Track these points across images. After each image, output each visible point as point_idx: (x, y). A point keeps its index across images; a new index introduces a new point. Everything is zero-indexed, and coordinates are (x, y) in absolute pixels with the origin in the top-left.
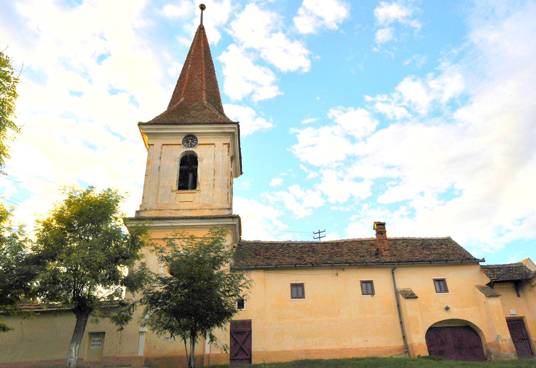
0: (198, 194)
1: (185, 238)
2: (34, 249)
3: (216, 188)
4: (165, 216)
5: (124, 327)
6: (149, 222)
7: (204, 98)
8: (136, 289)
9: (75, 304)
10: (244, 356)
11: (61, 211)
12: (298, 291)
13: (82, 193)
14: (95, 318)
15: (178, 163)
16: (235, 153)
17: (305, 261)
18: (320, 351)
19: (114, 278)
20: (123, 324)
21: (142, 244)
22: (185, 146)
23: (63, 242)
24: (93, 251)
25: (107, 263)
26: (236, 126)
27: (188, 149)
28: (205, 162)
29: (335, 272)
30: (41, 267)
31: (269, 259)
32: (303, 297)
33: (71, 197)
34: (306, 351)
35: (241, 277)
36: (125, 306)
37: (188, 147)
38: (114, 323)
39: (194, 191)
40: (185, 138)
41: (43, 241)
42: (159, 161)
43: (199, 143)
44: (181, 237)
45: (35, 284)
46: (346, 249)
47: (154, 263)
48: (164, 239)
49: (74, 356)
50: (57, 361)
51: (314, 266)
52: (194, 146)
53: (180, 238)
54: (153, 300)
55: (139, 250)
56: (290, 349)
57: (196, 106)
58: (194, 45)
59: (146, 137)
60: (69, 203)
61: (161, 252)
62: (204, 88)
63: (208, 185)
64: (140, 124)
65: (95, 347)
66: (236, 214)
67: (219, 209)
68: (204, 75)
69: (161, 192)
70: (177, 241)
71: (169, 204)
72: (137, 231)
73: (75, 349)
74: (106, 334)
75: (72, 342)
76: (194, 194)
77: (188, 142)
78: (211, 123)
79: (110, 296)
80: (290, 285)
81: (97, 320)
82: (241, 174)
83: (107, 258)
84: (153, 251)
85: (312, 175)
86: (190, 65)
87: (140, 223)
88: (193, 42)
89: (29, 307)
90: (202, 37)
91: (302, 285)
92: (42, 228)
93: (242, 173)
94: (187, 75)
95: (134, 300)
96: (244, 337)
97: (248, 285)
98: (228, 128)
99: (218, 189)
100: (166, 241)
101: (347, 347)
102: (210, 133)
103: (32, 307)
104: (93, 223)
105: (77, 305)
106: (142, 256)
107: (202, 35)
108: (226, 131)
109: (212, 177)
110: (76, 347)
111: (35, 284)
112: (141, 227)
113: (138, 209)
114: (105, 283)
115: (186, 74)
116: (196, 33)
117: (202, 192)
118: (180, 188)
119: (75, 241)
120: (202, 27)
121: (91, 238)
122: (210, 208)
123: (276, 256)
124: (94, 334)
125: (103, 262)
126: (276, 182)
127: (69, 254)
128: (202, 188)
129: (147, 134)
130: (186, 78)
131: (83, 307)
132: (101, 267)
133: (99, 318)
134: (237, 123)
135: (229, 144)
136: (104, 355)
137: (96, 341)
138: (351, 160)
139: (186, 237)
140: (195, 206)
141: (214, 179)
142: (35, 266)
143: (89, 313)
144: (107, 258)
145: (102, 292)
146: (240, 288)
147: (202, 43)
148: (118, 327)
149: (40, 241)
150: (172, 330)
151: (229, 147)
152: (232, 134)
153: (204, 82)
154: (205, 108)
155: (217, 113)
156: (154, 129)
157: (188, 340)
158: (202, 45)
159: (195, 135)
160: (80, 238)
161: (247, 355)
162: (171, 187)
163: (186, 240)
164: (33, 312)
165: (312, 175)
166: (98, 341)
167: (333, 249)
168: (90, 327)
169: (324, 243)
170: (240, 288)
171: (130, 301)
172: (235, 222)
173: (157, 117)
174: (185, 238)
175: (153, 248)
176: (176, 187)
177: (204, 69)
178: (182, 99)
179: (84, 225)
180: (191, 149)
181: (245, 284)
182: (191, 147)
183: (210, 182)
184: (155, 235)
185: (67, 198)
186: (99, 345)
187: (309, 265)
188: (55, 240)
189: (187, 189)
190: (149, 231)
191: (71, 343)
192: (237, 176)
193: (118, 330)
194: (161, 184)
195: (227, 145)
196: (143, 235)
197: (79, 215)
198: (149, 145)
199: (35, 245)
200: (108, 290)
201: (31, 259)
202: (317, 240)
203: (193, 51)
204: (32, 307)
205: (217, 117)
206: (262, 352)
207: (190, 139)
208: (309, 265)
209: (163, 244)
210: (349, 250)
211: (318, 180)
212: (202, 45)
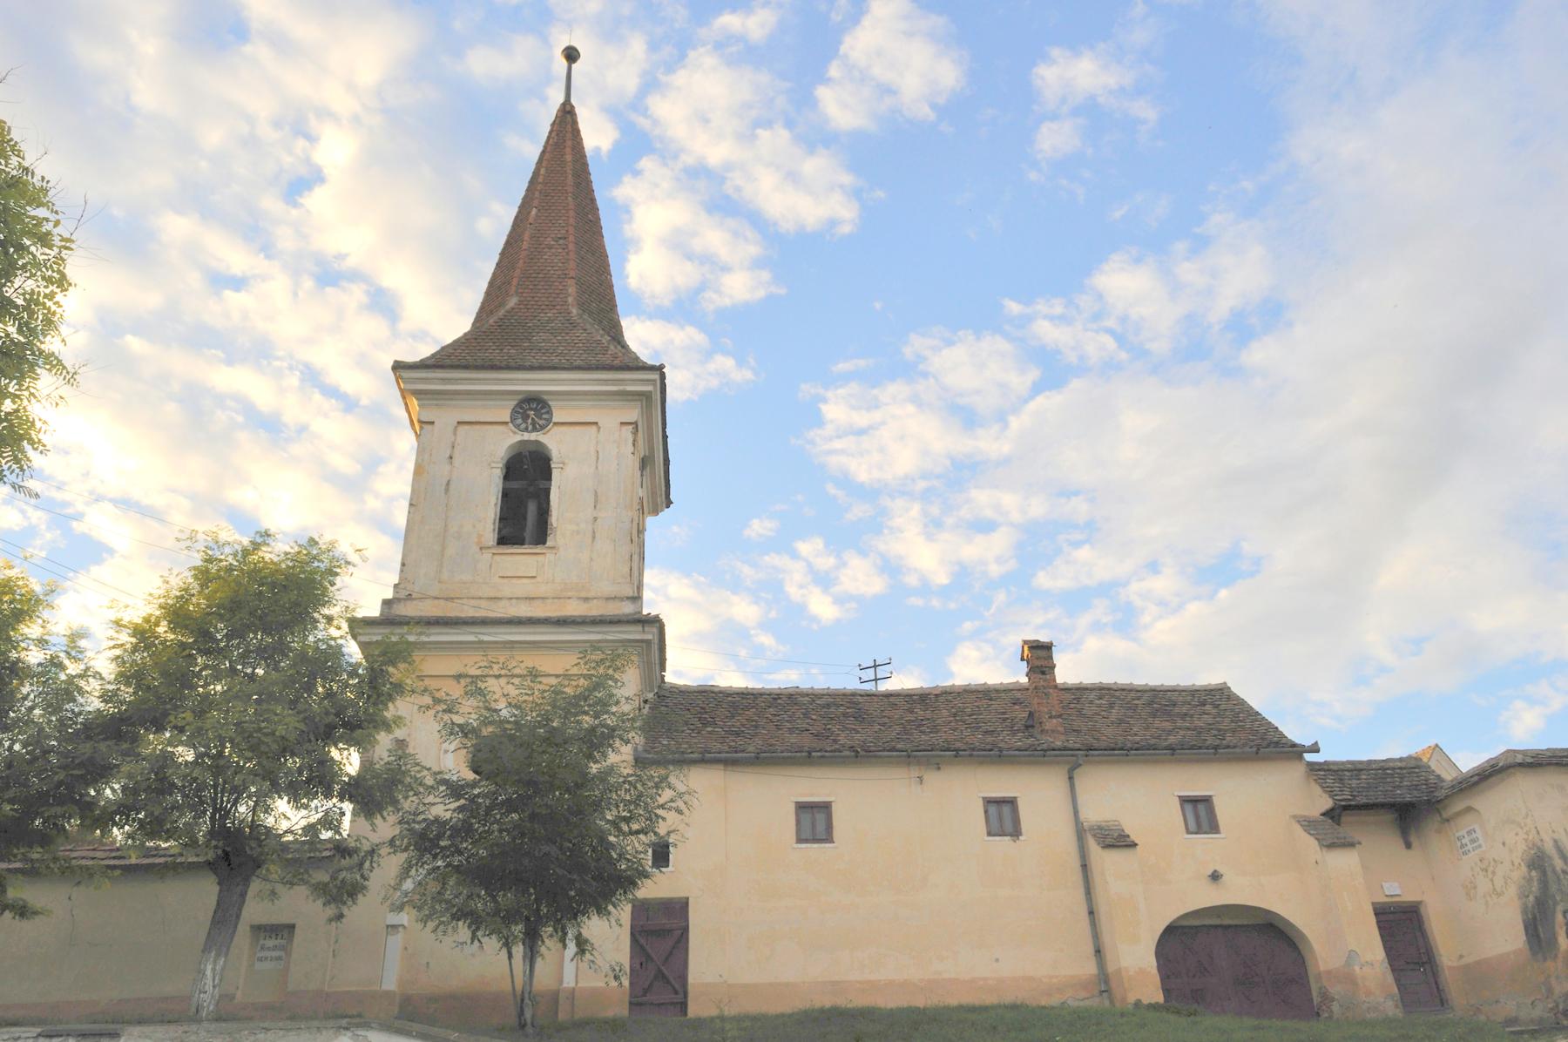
0: (550, 556)
1: (513, 676)
2: (106, 697)
5: (345, 911)
7: (570, 300)
9: (216, 847)
14: (269, 886)
15: (498, 473)
17: (835, 741)
19: (321, 780)
21: (399, 688)
22: (517, 427)
23: (185, 680)
24: (265, 706)
26: (656, 376)
27: (526, 436)
29: (915, 772)
30: (125, 746)
31: (738, 734)
32: (828, 838)
34: (834, 983)
38: (320, 902)
39: (539, 549)
42: (447, 467)
43: (555, 420)
45: (108, 792)
48: (458, 677)
51: (861, 756)
52: (542, 428)
54: (424, 840)
57: (550, 321)
58: (547, 156)
61: (449, 711)
62: (572, 274)
64: (398, 367)
67: (607, 599)
68: (571, 238)
70: (491, 681)
72: (384, 654)
73: (214, 970)
75: (206, 949)
76: (540, 558)
77: (525, 418)
79: (311, 829)
81: (273, 893)
83: (302, 726)
84: (428, 708)
86: (534, 211)
90: (569, 135)
92: (126, 638)
93: (669, 503)
94: (526, 237)
95: (375, 838)
97: (680, 804)
98: (634, 383)
101: (946, 976)
102: (586, 393)
103: (98, 854)
104: (266, 632)
105: (220, 852)
106: (398, 721)
107: (569, 128)
110: (215, 962)
111: (108, 792)
112: (396, 643)
114: (298, 792)
118: (502, 541)
119: (217, 678)
121: (260, 672)
122: (583, 595)
124: (261, 930)
125: (292, 737)
127: (200, 713)
129: (418, 394)
130: (525, 245)
131: (237, 857)
132: (286, 749)
133: (279, 888)
134: (661, 367)
135: (636, 424)
138: (963, 472)
140: (542, 590)
141: (595, 519)
144: (302, 726)
145: (288, 817)
147: (568, 150)
148: (331, 911)
149: (124, 678)
152: (646, 396)
154: (574, 325)
156: (435, 381)
157: (519, 950)
158: (569, 158)
160: (233, 670)
161: (676, 993)
162: (480, 536)
163: (516, 681)
165: (859, 511)
166: (275, 948)
168: (256, 909)
169: (888, 695)
172: (650, 634)
175: (427, 700)
176: (490, 537)
177: (571, 221)
178: (512, 302)
179: (242, 637)
180: (533, 436)
182: (535, 429)
185: (199, 563)
186: (279, 958)
190: (417, 656)
193: (330, 920)
196: (402, 666)
197: (231, 610)
198: (420, 422)
200: (304, 812)
203: (543, 171)
207: (533, 409)
210: (955, 715)
212: (569, 158)
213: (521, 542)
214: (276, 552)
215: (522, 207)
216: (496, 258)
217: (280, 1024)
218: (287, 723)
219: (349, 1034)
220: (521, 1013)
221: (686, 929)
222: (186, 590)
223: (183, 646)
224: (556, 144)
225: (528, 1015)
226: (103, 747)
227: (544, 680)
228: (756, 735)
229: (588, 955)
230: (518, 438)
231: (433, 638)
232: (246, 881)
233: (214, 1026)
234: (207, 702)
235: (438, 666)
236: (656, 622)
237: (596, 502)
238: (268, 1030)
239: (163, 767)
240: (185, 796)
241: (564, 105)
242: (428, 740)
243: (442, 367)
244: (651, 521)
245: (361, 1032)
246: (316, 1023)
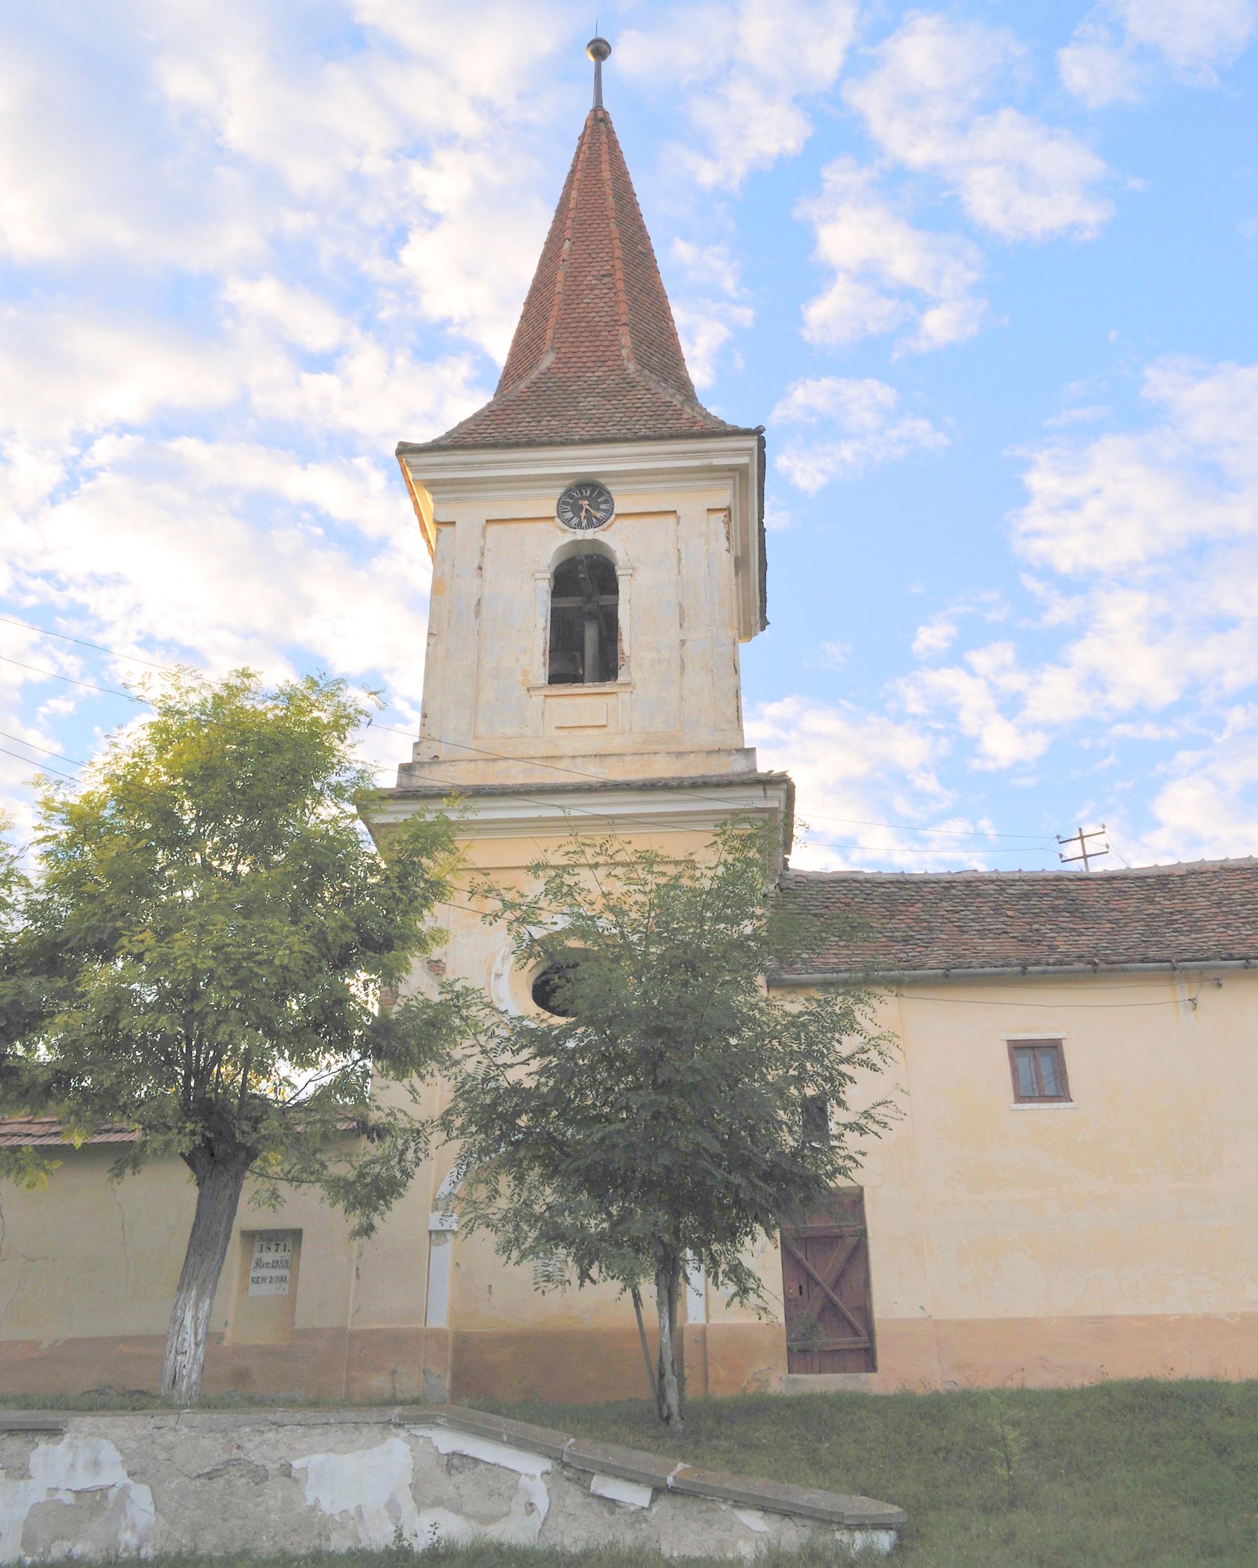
0: (624, 696)
1: (616, 864)
2: (35, 912)
4: (510, 782)
5: (376, 1220)
7: (624, 352)
8: (417, 1065)
9: (193, 1133)
10: (846, 1341)
11: (136, 765)
12: (1040, 1070)
13: (208, 695)
14: (268, 1185)
16: (745, 548)
17: (1052, 948)
19: (330, 1025)
20: (376, 1209)
21: (438, 890)
22: (567, 522)
23: (140, 884)
24: (256, 920)
25: (310, 969)
26: (752, 443)
27: (581, 535)
29: (1184, 992)
30: (61, 983)
31: (905, 941)
32: (1062, 1095)
33: (168, 712)
36: (380, 1137)
37: (579, 526)
38: (340, 1206)
39: (608, 687)
40: (568, 493)
41: (69, 881)
43: (616, 510)
44: (601, 859)
45: (42, 1048)
46: (1203, 902)
48: (536, 868)
49: (189, 1346)
50: (125, 1340)
51: (1098, 968)
52: (601, 522)
53: (596, 865)
54: (491, 1116)
55: (425, 912)
57: (600, 380)
58: (578, 175)
59: (426, 499)
60: (163, 737)
61: (522, 921)
62: (624, 319)
64: (404, 450)
65: (266, 1290)
66: (777, 770)
67: (709, 752)
68: (619, 275)
72: (415, 838)
73: (195, 1318)
77: (577, 510)
78: (661, 438)
79: (324, 1094)
81: (275, 1195)
82: (763, 629)
83: (310, 949)
85: (1061, 612)
89: (26, 1129)
90: (604, 147)
92: (63, 832)
93: (764, 623)
94: (560, 277)
95: (419, 1113)
96: (836, 1258)
100: (544, 875)
102: (657, 472)
103: (34, 1129)
105: (198, 1139)
106: (439, 936)
107: (604, 139)
111: (42, 1048)
112: (431, 824)
113: (408, 759)
114: (301, 1043)
115: (554, 273)
118: (554, 679)
119: (185, 882)
120: (600, 115)
121: (244, 869)
122: (675, 748)
123: (931, 929)
125: (297, 964)
126: (932, 636)
127: (164, 934)
129: (430, 485)
130: (559, 287)
131: (223, 1140)
133: (284, 1189)
134: (758, 433)
135: (728, 509)
137: (267, 1265)
138: (1198, 553)
139: (620, 857)
140: (615, 745)
141: (683, 642)
142: (42, 979)
144: (310, 949)
145: (294, 1080)
146: (844, 1068)
147: (605, 166)
148: (355, 1220)
150: (588, 1254)
152: (741, 471)
153: (622, 296)
154: (632, 385)
155: (677, 401)
157: (648, 1289)
158: (607, 175)
159: (602, 481)
160: (206, 866)
161: (856, 1334)
162: (525, 673)
163: (619, 871)
165: (1061, 612)
166: (275, 1265)
167: (1152, 902)
168: (250, 1212)
169: (1110, 879)
170: (844, 1068)
171: (400, 1115)
172: (774, 800)
173: (461, 425)
174: (616, 864)
175: (494, 905)
176: (540, 672)
177: (618, 253)
178: (548, 360)
179: (218, 819)
180: (589, 534)
182: (590, 525)
184: (479, 852)
185: (156, 718)
186: (282, 1279)
187: (1078, 966)
188: (111, 876)
189: (582, 681)
190: (461, 841)
191: (180, 1289)
193: (356, 1234)
195: (722, 515)
196: (441, 856)
197: (203, 779)
198: (438, 523)
199: (41, 897)
200: (311, 1072)
201: (25, 952)
202: (1076, 867)
203: (574, 194)
204: (34, 1129)
205: (679, 414)
207: (586, 498)
208: (1078, 966)
211: (1078, 630)
212: (607, 175)
213: (577, 679)
214: (262, 704)
215: (549, 243)
216: (520, 310)
217: (299, 1417)
218: (288, 944)
219: (403, 1434)
220: (661, 1396)
221: (864, 1233)
222: (141, 756)
223: (137, 834)
224: (588, 160)
225: (672, 1398)
226: (30, 985)
227: (663, 868)
228: (931, 942)
229: (752, 1295)
231: (483, 816)
232: (238, 1180)
233: (199, 1418)
235: (498, 852)
240: (148, 1053)
241: (595, 111)
242: (476, 956)
243: (463, 447)
245: (422, 1431)
246: (350, 1415)
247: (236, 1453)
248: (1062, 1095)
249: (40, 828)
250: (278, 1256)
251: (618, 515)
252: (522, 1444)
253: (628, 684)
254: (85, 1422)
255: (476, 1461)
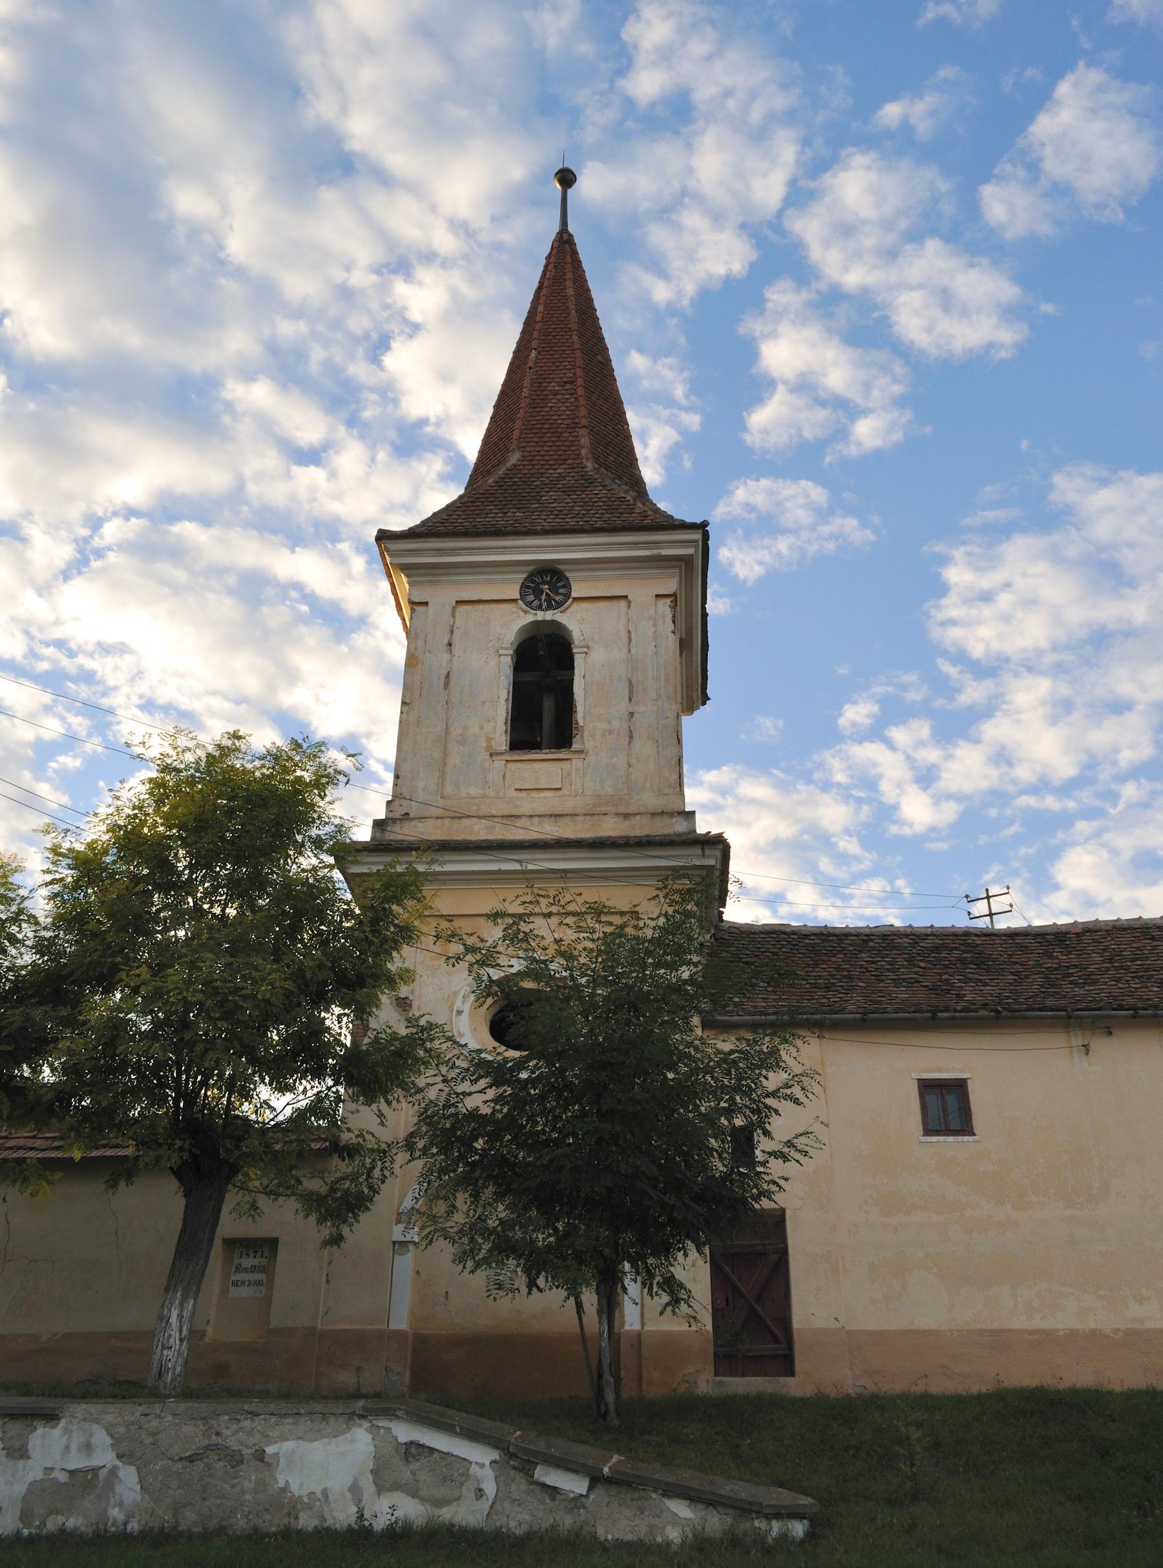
0: (577, 763)
2: (41, 947)
3: (637, 744)
4: (473, 838)
5: (345, 1231)
6: (427, 857)
7: (583, 452)
8: (385, 1092)
9: (181, 1149)
12: (947, 1107)
15: (507, 662)
17: (960, 997)
18: (1046, 1339)
19: (306, 1054)
21: (407, 934)
22: (529, 604)
26: (698, 536)
27: (541, 616)
28: (598, 655)
29: (1078, 1040)
30: (64, 1012)
31: (828, 988)
33: (166, 769)
34: (995, 1333)
35: (772, 1061)
36: (351, 1156)
37: (540, 608)
38: (313, 1218)
40: (530, 578)
41: (71, 918)
42: (446, 656)
43: (574, 594)
44: (554, 909)
45: (47, 1070)
46: (1096, 957)
47: (442, 995)
48: (495, 916)
49: (174, 1341)
52: (559, 605)
53: (550, 915)
54: (447, 1134)
56: (934, 1326)
57: (561, 477)
58: (544, 291)
61: (482, 963)
62: (584, 422)
63: (610, 732)
64: (383, 536)
65: (245, 1292)
67: (654, 814)
68: (580, 382)
69: (454, 759)
70: (539, 922)
71: (484, 796)
72: (386, 886)
73: (180, 1316)
74: (281, 1255)
75: (170, 1287)
76: (565, 765)
77: (538, 593)
79: (300, 1117)
80: (915, 1084)
81: (254, 1206)
82: (704, 704)
83: (289, 985)
84: (459, 959)
85: (973, 693)
86: (533, 354)
87: (394, 862)
88: (541, 283)
90: (569, 267)
91: (959, 1087)
92: (68, 874)
93: (705, 699)
94: (526, 383)
95: (385, 1135)
97: (796, 1091)
98: (671, 546)
99: (643, 748)
101: (1149, 1325)
103: (38, 1143)
104: (238, 861)
105: (186, 1156)
106: (407, 976)
107: (568, 259)
108: (665, 552)
109: (623, 706)
110: (182, 1306)
111: (47, 1070)
112: (401, 874)
113: (382, 815)
116: (548, 258)
117: (592, 757)
119: (177, 923)
120: (565, 237)
121: (231, 912)
122: (622, 810)
124: (238, 1245)
126: (857, 713)
127: (159, 970)
128: (589, 744)
129: (406, 568)
131: (211, 1153)
132: (269, 1018)
133: (263, 1201)
134: (703, 527)
135: (674, 595)
136: (275, 1323)
137: (246, 1270)
138: (1099, 642)
139: (571, 908)
140: (570, 805)
141: (631, 714)
143: (228, 1180)
144: (289, 985)
145: (275, 1104)
146: (770, 1101)
147: (569, 283)
148: (326, 1231)
149: (62, 921)
150: (537, 1264)
151: (674, 606)
152: (687, 561)
153: (582, 402)
154: (590, 481)
156: (429, 553)
157: (590, 1298)
158: (570, 292)
159: (561, 567)
160: (197, 908)
162: (489, 740)
163: (570, 920)
164: (41, 1161)
165: (973, 693)
166: (253, 1270)
167: (1051, 957)
168: (230, 1224)
170: (770, 1101)
171: (368, 1137)
173: (435, 514)
175: (456, 948)
176: (501, 740)
177: (579, 362)
178: (514, 458)
179: (209, 867)
180: (549, 615)
181: (787, 1086)
182: (550, 607)
183: (616, 724)
184: (445, 902)
185: (154, 775)
186: (259, 1283)
189: (540, 749)
190: (428, 890)
191: (167, 1290)
192: (690, 708)
193: (326, 1243)
194: (456, 731)
195: (668, 600)
196: (410, 903)
200: (289, 1096)
203: (540, 308)
206: (825, 1331)
207: (546, 583)
209: (494, 933)
210: (1111, 960)
211: (988, 710)
212: (570, 292)
213: (534, 746)
216: (490, 411)
217: (272, 1407)
218: (271, 979)
219: (366, 1425)
220: (600, 1394)
221: (784, 1252)
222: (140, 808)
223: (136, 879)
225: (610, 1396)
226: (37, 1014)
228: (851, 989)
230: (530, 618)
233: (182, 1407)
234: (167, 953)
236: (719, 845)
237: (631, 693)
238: (255, 1414)
239: (114, 1038)
244: (685, 719)
247: (215, 1439)
248: (966, 1128)
249: (48, 872)
250: (256, 1261)
251: (576, 599)
252: (473, 1435)
253: (582, 752)
254: (80, 1409)
255: (432, 1450)
